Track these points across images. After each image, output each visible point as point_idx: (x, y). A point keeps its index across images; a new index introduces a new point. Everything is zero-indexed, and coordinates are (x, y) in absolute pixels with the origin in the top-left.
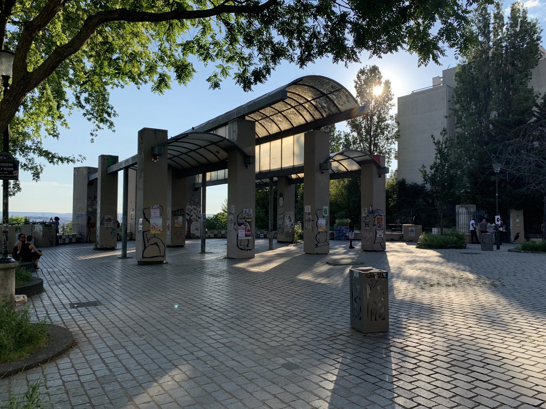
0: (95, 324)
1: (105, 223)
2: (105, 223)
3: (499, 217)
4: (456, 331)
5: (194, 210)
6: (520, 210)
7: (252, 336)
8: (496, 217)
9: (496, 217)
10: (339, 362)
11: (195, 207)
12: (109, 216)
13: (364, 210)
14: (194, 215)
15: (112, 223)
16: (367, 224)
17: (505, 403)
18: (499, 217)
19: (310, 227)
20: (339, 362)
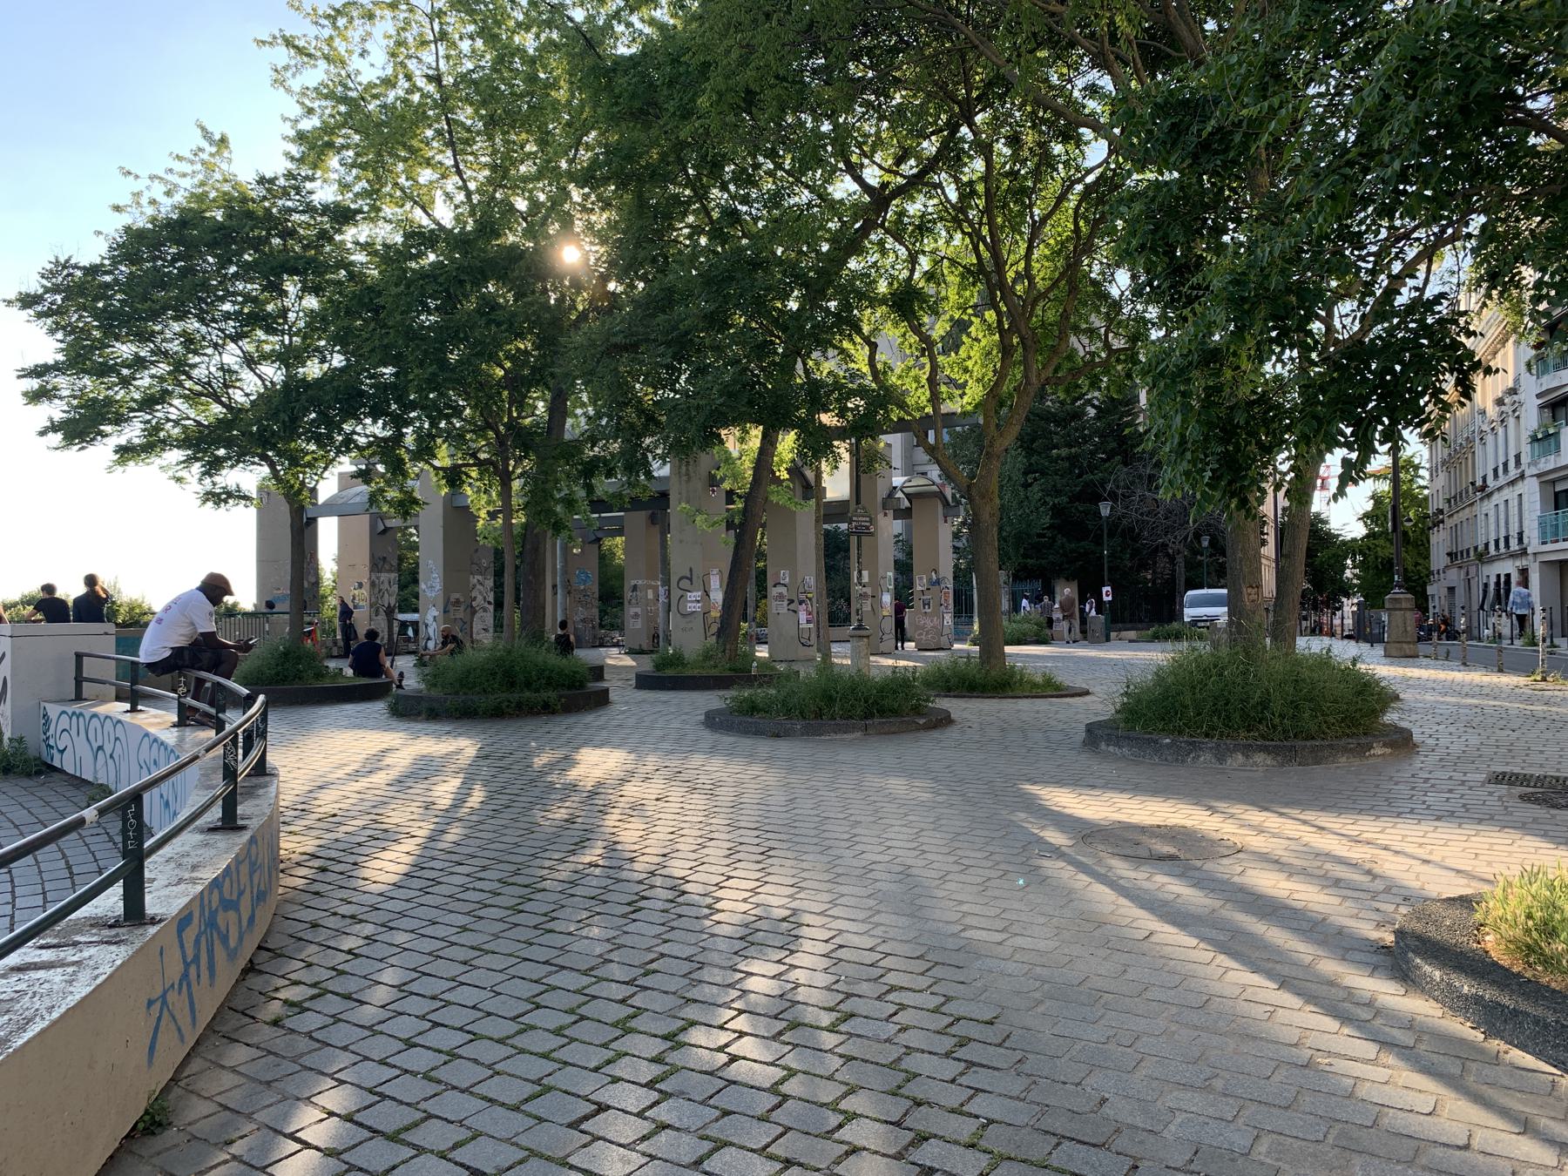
0: (575, 805)
1: (452, 608)
2: (452, 608)
3: (1109, 588)
4: (836, 862)
5: (478, 586)
6: (168, 609)
7: (349, 921)
8: (1105, 589)
9: (1105, 589)
10: (233, 1070)
11: (480, 578)
12: (457, 595)
13: (921, 579)
14: (480, 598)
15: (462, 608)
16: (926, 604)
17: (938, 1036)
18: (1109, 588)
19: (869, 609)
20: (233, 1070)
